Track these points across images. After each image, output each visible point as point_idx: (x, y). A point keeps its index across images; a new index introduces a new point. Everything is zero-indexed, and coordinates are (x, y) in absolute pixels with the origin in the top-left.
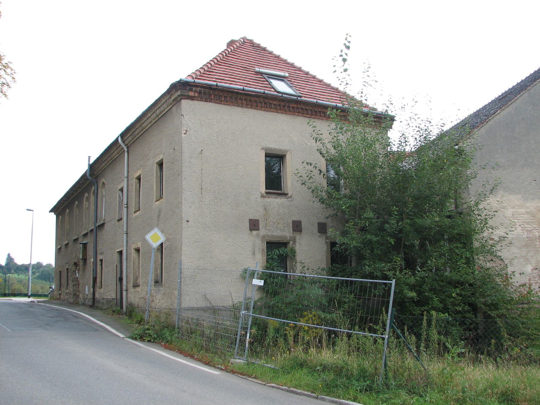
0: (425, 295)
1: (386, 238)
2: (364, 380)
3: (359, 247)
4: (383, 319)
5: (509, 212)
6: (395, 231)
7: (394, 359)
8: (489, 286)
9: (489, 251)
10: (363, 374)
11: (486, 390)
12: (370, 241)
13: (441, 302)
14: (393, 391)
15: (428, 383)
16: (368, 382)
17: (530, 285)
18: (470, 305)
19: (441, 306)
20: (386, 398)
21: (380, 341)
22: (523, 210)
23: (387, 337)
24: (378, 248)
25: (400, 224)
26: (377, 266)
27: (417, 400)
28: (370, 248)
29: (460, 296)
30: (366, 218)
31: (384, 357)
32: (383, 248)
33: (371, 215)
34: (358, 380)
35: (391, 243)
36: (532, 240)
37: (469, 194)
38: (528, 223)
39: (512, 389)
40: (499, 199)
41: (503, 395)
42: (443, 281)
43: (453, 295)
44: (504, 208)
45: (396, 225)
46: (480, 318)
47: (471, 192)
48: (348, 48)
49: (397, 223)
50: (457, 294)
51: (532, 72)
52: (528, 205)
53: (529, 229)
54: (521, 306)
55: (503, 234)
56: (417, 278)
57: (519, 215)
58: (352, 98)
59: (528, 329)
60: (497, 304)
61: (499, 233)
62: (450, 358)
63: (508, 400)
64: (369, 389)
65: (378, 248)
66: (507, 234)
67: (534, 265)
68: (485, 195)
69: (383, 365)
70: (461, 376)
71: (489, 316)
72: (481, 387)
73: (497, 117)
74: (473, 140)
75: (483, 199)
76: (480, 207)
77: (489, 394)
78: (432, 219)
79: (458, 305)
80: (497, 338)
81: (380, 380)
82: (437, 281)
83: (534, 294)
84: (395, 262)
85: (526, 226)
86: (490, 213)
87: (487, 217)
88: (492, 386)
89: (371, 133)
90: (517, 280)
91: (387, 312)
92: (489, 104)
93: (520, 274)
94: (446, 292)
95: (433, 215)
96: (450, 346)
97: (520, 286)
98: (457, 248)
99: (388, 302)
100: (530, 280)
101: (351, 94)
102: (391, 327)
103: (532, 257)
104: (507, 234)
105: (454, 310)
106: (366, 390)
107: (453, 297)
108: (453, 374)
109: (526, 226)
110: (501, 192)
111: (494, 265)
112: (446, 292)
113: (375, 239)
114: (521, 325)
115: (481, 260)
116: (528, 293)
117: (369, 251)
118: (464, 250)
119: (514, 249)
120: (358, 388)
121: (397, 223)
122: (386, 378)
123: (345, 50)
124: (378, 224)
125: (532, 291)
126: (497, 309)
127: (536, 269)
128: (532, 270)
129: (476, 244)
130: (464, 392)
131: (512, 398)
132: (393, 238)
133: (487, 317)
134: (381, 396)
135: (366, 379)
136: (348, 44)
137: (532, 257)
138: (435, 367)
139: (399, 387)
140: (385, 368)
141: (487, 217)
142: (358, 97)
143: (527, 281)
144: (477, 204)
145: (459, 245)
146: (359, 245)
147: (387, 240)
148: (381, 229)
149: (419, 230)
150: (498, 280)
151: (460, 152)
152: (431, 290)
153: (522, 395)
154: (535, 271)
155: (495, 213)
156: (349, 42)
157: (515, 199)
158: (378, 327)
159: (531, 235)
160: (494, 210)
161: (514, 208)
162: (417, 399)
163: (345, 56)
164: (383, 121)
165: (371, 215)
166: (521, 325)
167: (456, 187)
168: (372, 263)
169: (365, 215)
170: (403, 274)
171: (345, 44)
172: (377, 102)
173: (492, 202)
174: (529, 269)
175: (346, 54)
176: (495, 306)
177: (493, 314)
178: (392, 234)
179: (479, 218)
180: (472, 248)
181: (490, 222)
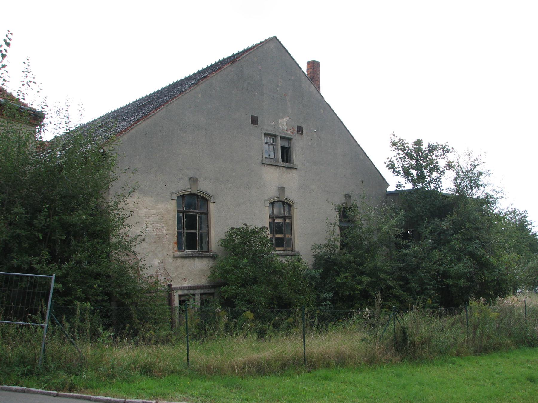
0: (69, 286)
1: (34, 233)
2: (24, 365)
3: (9, 241)
4: (42, 310)
5: (142, 212)
6: (44, 226)
7: (54, 345)
8: (125, 278)
9: (127, 249)
10: (23, 361)
11: (129, 365)
12: (19, 236)
13: (83, 293)
14: (53, 372)
15: (83, 363)
16: (29, 367)
17: (157, 276)
18: (107, 294)
19: (83, 296)
20: (47, 379)
21: (39, 328)
22: (154, 211)
23: (46, 325)
24: (26, 241)
25: (48, 220)
26: (25, 259)
27: (75, 378)
28: (18, 241)
29: (101, 287)
30: (15, 213)
31: (43, 343)
32: (30, 242)
33: (22, 211)
34: (18, 366)
35: (39, 237)
36: (160, 237)
37: (109, 194)
38: (157, 222)
39: (151, 363)
40: (135, 200)
41: (143, 369)
42: (85, 274)
43: (95, 286)
44: (138, 208)
45: (44, 221)
46: (114, 307)
47: (111, 192)
48: (8, 45)
49: (46, 219)
50: (99, 286)
51: (168, 85)
52: (159, 206)
53: (158, 227)
54: (148, 295)
55: (139, 233)
56: (64, 271)
57: (151, 215)
58: (10, 95)
59: (155, 314)
60: (130, 293)
61: (137, 230)
62: (101, 341)
63: (147, 372)
64: (30, 373)
65: (26, 241)
66: (143, 233)
67: (161, 259)
68: (124, 196)
69: (42, 350)
70: (110, 355)
71: (123, 305)
72: (126, 363)
73: (138, 127)
74: (116, 147)
75: (122, 200)
76: (120, 206)
77: (132, 369)
78: (79, 217)
79: (98, 295)
80: (130, 323)
81: (39, 364)
82: (80, 273)
83: (160, 284)
84: (43, 256)
85: (156, 225)
86: (127, 213)
87: (124, 216)
88: (135, 362)
89: (25, 129)
90: (146, 273)
91: (46, 303)
92: (127, 106)
93: (150, 267)
94: (87, 282)
95: (80, 214)
96: (101, 331)
97: (148, 277)
98: (98, 243)
99: (49, 294)
100: (157, 272)
101: (8, 91)
102: (51, 317)
103: (159, 252)
104: (143, 233)
105: (94, 299)
106: (27, 374)
107: (95, 289)
108: (103, 355)
109: (156, 225)
110: (136, 194)
111: (128, 259)
112: (87, 282)
113: (24, 233)
114: (149, 312)
115: (118, 255)
116: (155, 283)
117: (17, 245)
118: (104, 245)
119: (144, 245)
120: (19, 373)
121: (46, 219)
122: (45, 362)
123: (5, 47)
124: (27, 219)
125: (159, 281)
126: (130, 297)
127: (163, 262)
128: (159, 263)
129: (113, 240)
130: (113, 368)
131: (150, 370)
132: (41, 233)
133: (120, 304)
134: (41, 378)
135: (26, 364)
136: (8, 41)
137: (159, 252)
138: (87, 350)
139: (58, 368)
140: (44, 353)
141: (124, 216)
142: (15, 95)
143: (154, 273)
144: (116, 204)
145: (100, 241)
146: (8, 239)
147: (35, 235)
148: (30, 224)
149: (66, 227)
150: (131, 272)
151: (105, 155)
152: (73, 281)
153: (158, 366)
154: (161, 264)
155: (132, 213)
156: (10, 39)
157: (148, 201)
158: (36, 317)
159: (159, 233)
160: (131, 209)
161: (147, 208)
162: (75, 378)
163: (4, 53)
164: (36, 118)
165: (22, 211)
166: (149, 312)
167: (99, 187)
168: (19, 256)
169: (15, 210)
170: (49, 266)
171: (5, 41)
172: (32, 100)
173: (130, 203)
174: (156, 262)
175: (6, 51)
176: (128, 295)
177: (127, 302)
178: (40, 228)
179: (117, 216)
180: (109, 243)
181: (127, 222)
